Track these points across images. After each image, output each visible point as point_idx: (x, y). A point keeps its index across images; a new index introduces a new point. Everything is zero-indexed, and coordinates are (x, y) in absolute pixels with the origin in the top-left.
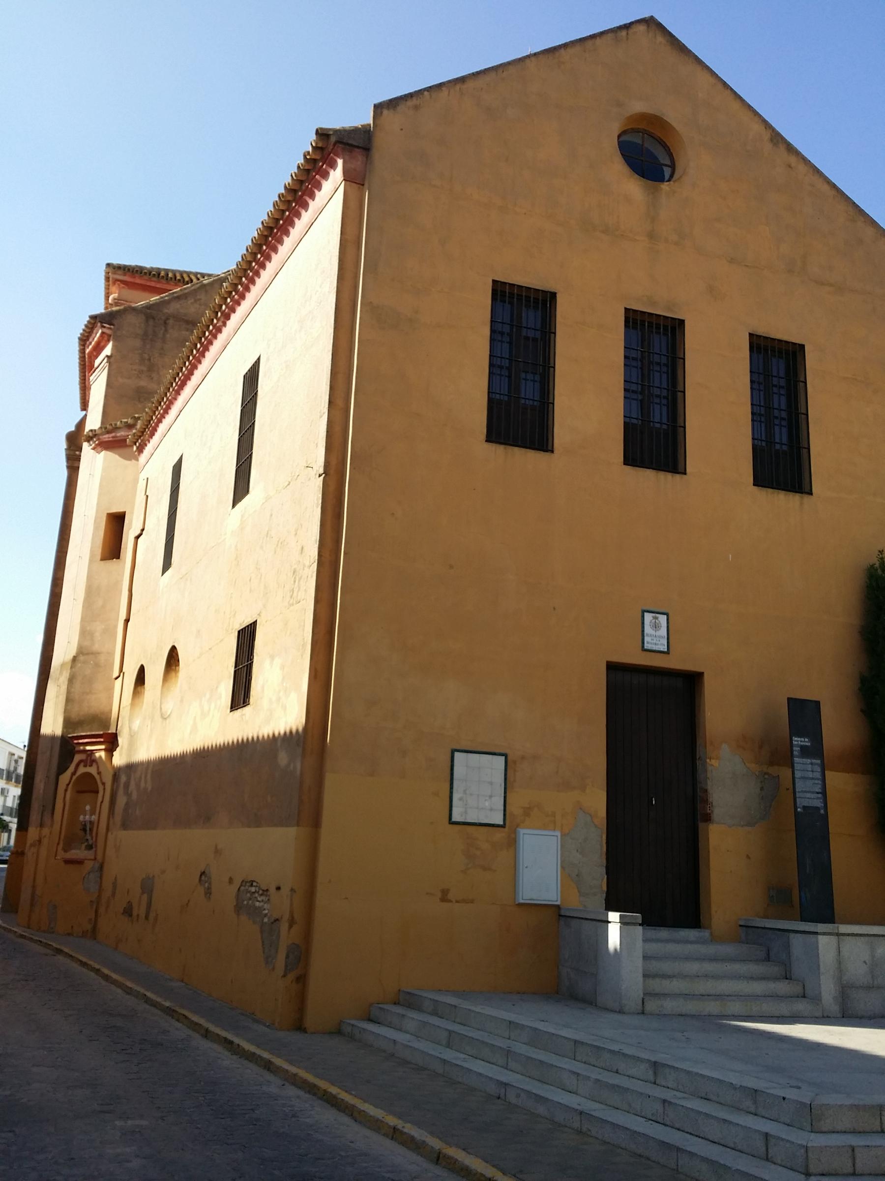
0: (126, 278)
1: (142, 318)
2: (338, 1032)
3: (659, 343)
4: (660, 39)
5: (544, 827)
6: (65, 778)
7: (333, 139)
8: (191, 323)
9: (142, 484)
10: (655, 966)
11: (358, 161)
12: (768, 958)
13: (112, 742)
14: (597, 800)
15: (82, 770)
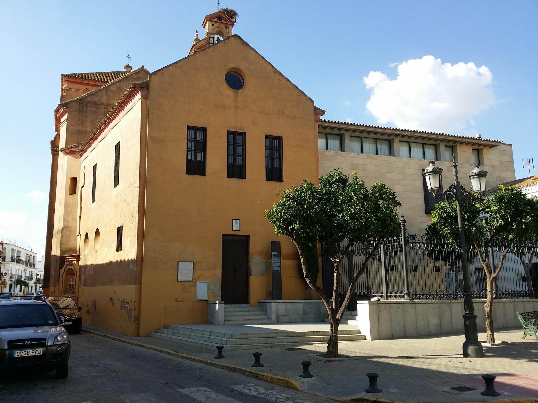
0: (70, 80)
1: (78, 104)
2: (148, 336)
3: (239, 138)
4: (239, 41)
5: (204, 280)
6: (62, 270)
7: (137, 86)
9: (82, 168)
10: (227, 314)
11: (145, 92)
12: (263, 310)
13: (78, 258)
14: (219, 272)
15: (68, 267)
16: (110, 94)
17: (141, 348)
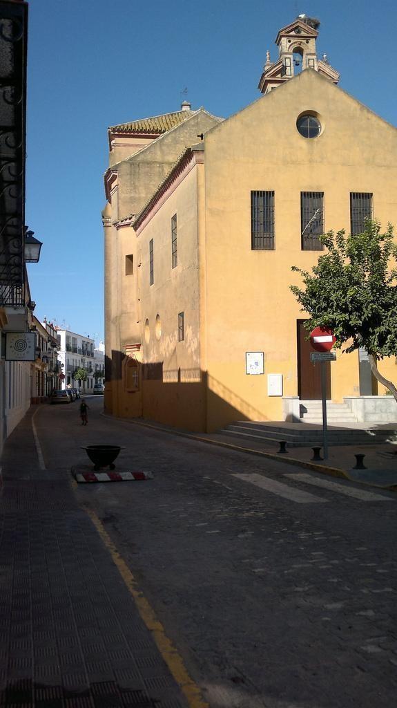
16: (164, 148)
17: (207, 445)
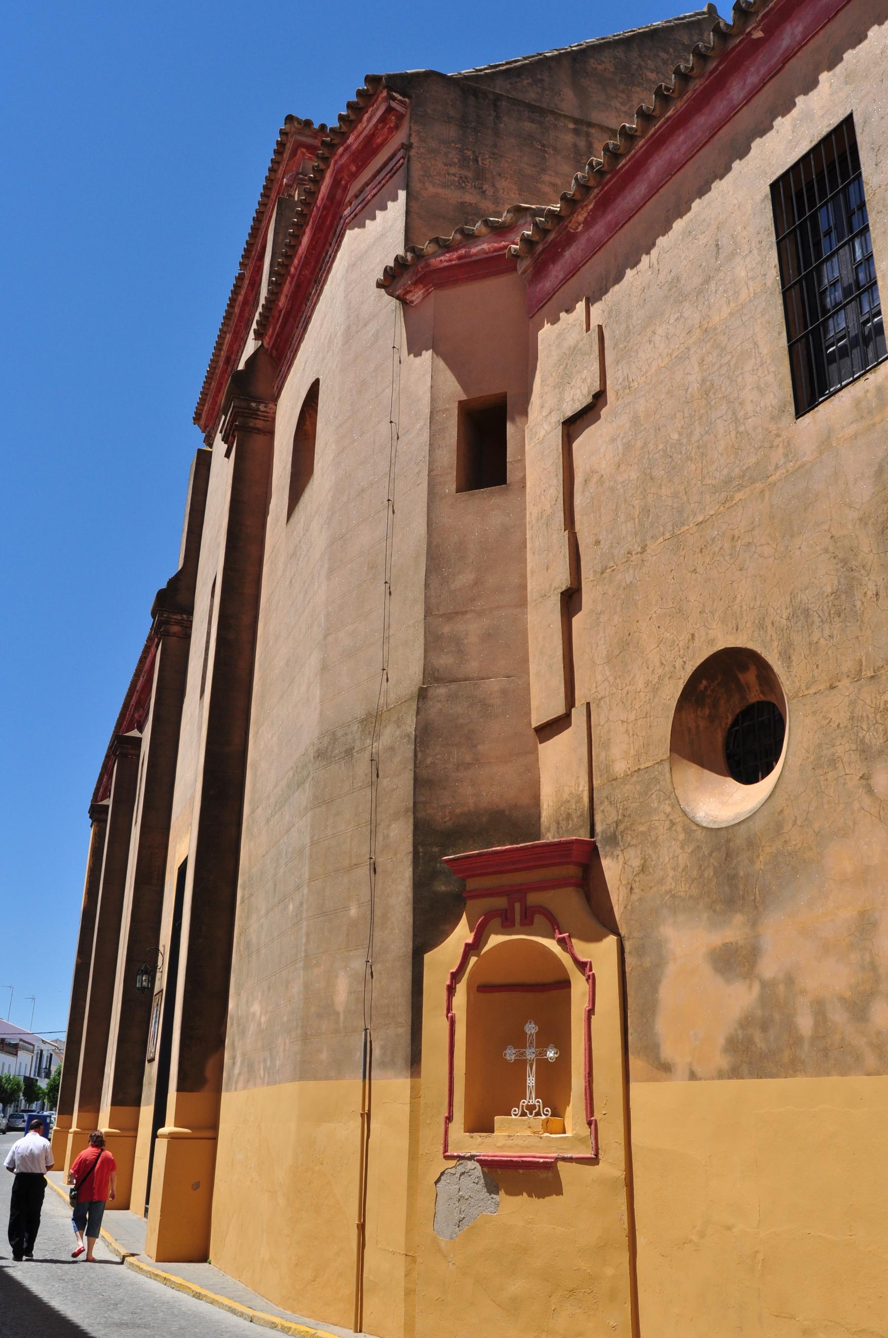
8: (537, 111)
